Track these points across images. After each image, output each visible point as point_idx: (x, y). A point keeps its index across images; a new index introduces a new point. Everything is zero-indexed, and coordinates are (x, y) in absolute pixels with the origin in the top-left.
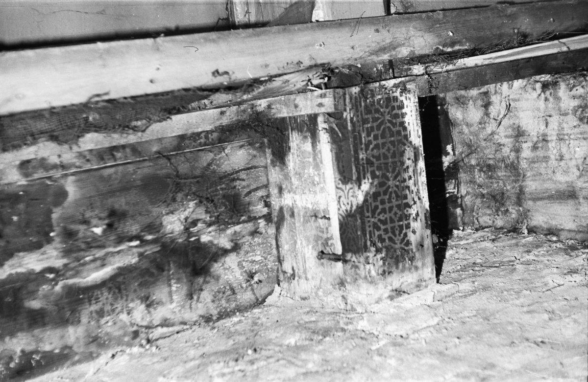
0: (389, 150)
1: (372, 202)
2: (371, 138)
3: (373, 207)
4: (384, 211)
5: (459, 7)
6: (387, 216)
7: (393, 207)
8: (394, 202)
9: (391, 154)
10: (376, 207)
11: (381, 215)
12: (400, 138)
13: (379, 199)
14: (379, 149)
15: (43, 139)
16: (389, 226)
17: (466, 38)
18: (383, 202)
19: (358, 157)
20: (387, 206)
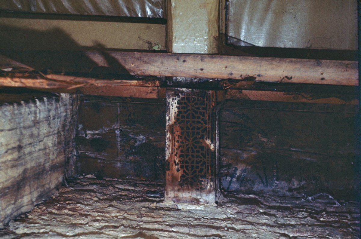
0: (190, 159)
1: (204, 169)
2: (200, 167)
3: (204, 166)
4: (198, 129)
5: (119, 48)
6: (195, 159)
7: (191, 163)
8: (190, 165)
9: (189, 157)
10: (202, 165)
11: (199, 160)
12: (182, 119)
13: (200, 150)
14: (196, 161)
15: (309, 217)
16: (196, 120)
17: (135, 175)
18: (197, 167)
19: (211, 126)
20: (195, 165)
